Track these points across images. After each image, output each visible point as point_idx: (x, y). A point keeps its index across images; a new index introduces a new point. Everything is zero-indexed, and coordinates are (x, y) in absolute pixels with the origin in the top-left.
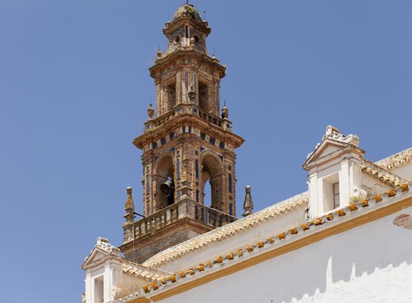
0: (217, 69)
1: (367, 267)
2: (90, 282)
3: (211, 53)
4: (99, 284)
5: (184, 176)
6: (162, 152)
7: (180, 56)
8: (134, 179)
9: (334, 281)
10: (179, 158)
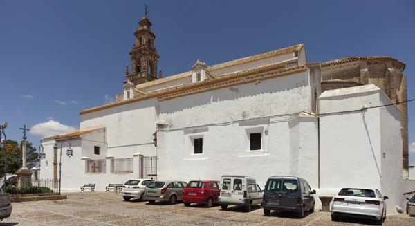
0: (153, 36)
1: (222, 99)
2: (125, 92)
3: (152, 31)
4: (128, 93)
5: (144, 64)
6: (137, 57)
7: (143, 31)
8: (130, 64)
9: (213, 101)
10: (143, 59)
